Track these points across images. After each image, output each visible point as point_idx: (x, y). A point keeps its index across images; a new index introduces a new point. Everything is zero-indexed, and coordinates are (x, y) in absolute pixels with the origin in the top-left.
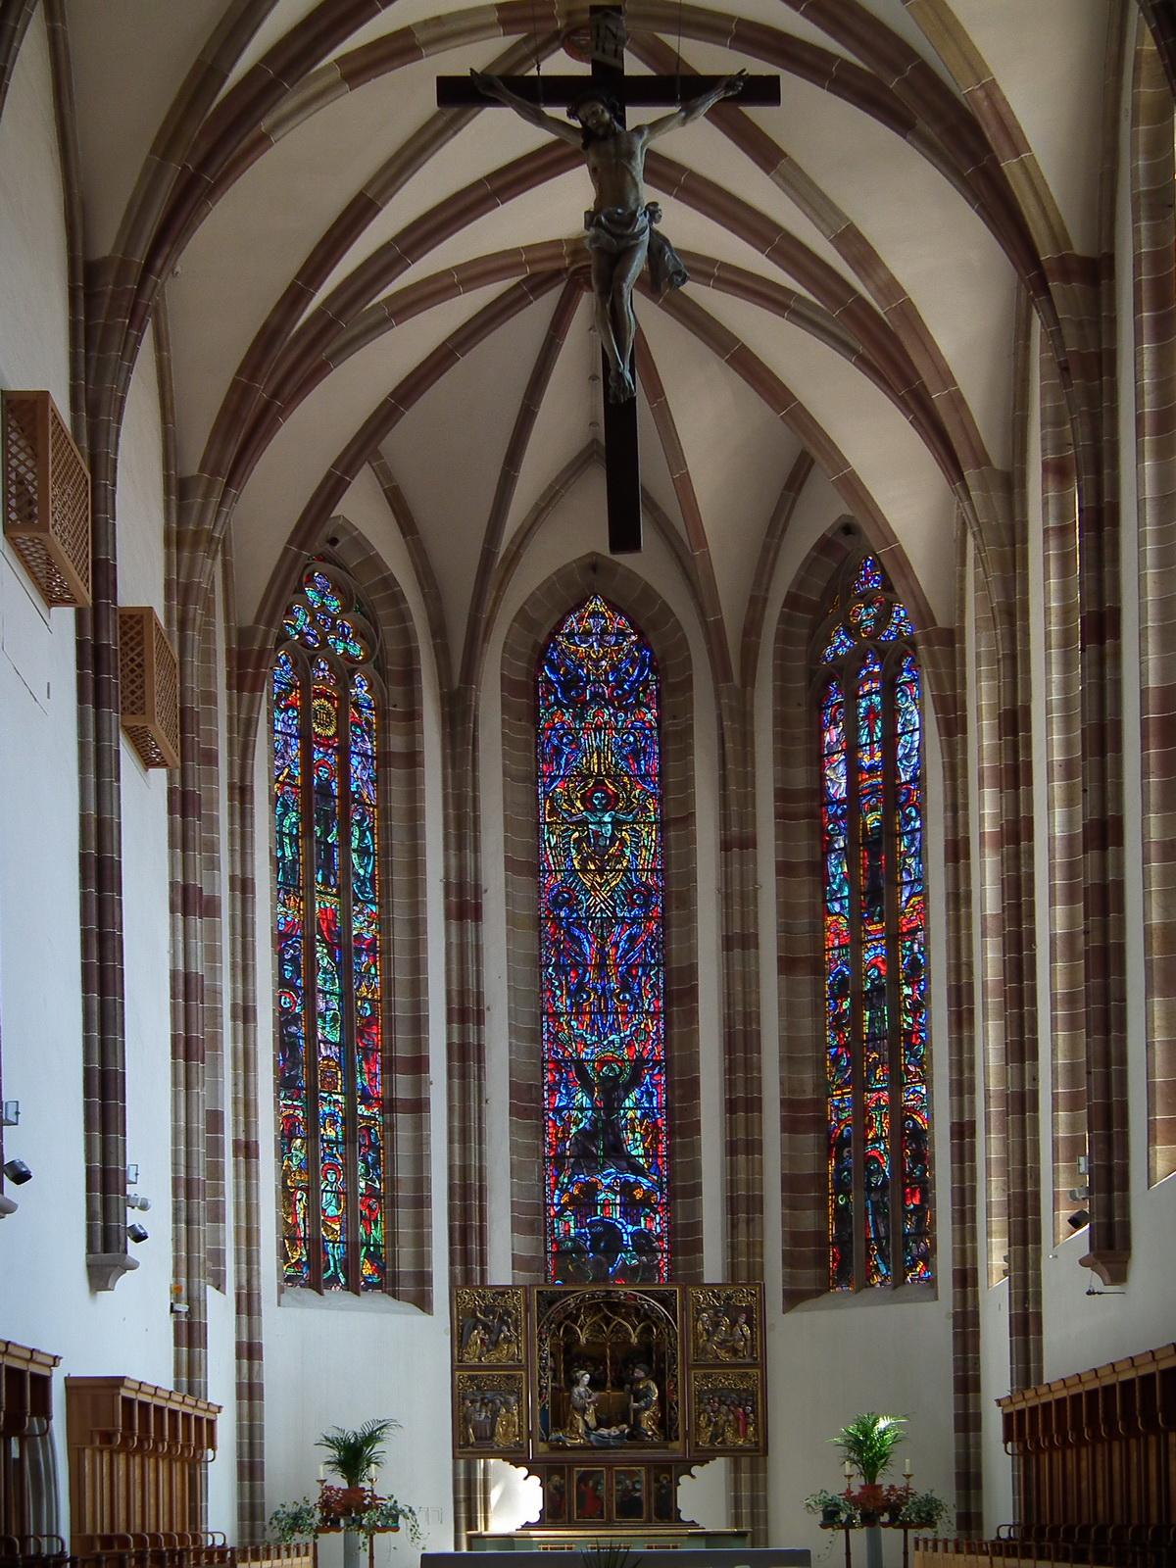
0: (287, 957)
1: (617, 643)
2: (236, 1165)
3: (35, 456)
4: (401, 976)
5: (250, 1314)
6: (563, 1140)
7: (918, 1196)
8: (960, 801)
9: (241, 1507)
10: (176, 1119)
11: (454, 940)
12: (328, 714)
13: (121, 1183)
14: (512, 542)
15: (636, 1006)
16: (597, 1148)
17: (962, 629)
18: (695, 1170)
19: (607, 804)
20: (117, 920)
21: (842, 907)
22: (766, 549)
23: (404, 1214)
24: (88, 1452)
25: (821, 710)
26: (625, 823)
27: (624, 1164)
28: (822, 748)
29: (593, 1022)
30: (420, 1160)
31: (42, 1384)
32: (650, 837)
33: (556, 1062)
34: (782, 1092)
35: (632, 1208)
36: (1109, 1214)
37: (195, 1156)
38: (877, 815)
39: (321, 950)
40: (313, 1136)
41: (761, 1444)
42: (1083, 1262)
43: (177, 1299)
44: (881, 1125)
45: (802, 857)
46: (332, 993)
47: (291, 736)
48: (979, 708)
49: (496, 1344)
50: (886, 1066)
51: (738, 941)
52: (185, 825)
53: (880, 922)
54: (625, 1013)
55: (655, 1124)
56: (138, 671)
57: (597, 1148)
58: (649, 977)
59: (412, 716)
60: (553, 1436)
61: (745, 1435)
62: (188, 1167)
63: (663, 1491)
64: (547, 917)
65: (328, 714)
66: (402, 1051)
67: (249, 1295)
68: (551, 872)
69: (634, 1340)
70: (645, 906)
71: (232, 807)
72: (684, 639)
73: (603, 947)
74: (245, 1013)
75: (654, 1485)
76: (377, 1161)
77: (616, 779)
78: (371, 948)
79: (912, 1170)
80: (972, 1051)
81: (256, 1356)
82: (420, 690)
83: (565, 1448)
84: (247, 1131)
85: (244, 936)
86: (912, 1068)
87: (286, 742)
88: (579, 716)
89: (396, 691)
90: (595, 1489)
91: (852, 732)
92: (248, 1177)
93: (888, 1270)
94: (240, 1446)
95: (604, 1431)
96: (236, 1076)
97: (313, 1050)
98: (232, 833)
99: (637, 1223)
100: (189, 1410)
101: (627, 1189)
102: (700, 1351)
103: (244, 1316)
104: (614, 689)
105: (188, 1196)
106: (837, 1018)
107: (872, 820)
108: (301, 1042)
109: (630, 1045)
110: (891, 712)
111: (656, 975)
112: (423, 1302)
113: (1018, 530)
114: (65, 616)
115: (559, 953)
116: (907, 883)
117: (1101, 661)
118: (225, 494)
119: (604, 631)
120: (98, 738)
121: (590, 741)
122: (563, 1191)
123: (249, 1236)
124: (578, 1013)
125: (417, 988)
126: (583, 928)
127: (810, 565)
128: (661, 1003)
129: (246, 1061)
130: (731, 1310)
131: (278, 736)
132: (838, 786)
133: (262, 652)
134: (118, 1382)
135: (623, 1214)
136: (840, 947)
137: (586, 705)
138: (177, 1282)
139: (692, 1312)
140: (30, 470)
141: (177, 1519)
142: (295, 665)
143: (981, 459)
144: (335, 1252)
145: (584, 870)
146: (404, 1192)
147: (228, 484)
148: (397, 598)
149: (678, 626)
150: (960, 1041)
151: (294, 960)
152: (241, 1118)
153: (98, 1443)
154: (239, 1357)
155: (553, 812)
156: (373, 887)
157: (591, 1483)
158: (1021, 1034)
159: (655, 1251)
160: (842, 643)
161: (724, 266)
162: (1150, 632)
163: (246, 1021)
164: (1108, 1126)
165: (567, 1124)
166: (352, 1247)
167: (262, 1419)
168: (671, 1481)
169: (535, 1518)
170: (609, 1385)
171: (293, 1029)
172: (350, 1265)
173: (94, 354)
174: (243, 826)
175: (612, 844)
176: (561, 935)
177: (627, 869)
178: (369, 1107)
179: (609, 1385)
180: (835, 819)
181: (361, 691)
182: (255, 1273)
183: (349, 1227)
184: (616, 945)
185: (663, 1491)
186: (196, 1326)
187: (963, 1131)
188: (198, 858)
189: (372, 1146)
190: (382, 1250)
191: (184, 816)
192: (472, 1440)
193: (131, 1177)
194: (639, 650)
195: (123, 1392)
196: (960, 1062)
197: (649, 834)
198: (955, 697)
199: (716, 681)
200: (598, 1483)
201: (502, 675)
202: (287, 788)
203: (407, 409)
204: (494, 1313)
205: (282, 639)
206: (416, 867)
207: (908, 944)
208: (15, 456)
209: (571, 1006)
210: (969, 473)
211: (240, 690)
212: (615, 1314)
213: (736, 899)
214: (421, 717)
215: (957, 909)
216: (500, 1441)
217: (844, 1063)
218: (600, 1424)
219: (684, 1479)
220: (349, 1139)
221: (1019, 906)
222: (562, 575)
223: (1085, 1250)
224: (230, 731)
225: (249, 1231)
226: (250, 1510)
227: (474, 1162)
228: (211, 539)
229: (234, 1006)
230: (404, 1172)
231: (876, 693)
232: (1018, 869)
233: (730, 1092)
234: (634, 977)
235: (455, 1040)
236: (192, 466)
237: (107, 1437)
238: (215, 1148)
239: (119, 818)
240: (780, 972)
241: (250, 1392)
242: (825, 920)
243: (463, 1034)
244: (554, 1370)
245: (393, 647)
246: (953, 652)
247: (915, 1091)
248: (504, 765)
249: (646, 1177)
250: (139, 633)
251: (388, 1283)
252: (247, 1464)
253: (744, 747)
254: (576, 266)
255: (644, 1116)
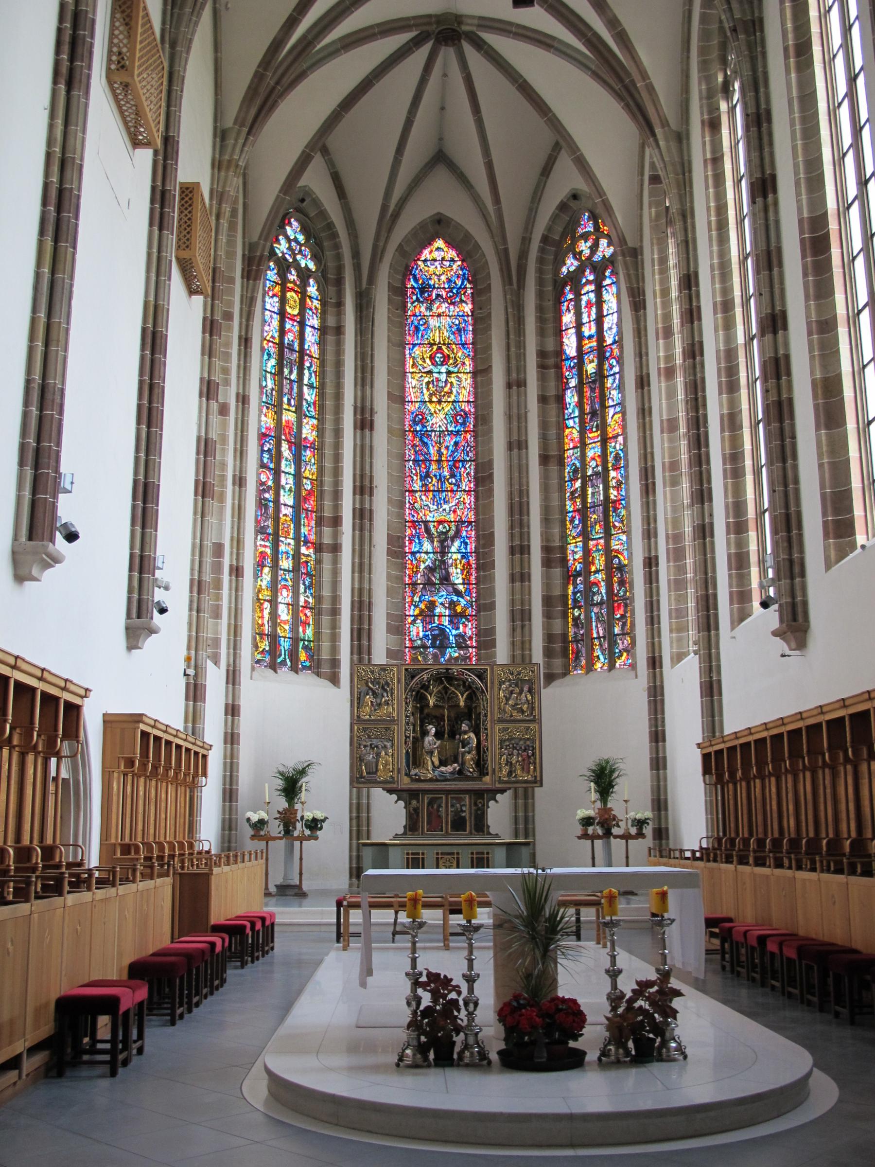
0: (266, 449)
1: (450, 266)
2: (231, 581)
3: (129, 37)
4: (328, 464)
5: (234, 684)
6: (417, 572)
7: (622, 609)
8: (644, 350)
9: (223, 821)
10: (194, 537)
11: (358, 442)
12: (295, 301)
13: (152, 567)
14: (396, 206)
15: (458, 486)
16: (435, 577)
17: (641, 247)
18: (491, 592)
19: (444, 361)
20: (162, 374)
21: (574, 422)
22: (530, 210)
23: (326, 619)
24: (116, 774)
25: (560, 303)
26: (453, 373)
27: (451, 589)
28: (561, 326)
29: (434, 496)
30: (335, 584)
31: (73, 711)
32: (467, 381)
33: (413, 522)
34: (542, 541)
35: (456, 617)
36: (793, 595)
37: (204, 564)
38: (594, 365)
39: (285, 446)
40: (275, 567)
41: (538, 779)
42: (775, 634)
43: (189, 667)
44: (599, 562)
45: (552, 392)
46: (289, 474)
47: (274, 312)
48: (654, 292)
49: (380, 705)
50: (602, 523)
51: (516, 445)
52: (211, 340)
53: (597, 431)
54: (452, 491)
55: (468, 563)
56: (189, 223)
57: (435, 577)
58: (466, 469)
59: (340, 304)
60: (413, 772)
61: (528, 772)
62: (200, 572)
63: (479, 812)
64: (410, 431)
65: (295, 301)
66: (327, 513)
67: (234, 671)
68: (412, 402)
69: (462, 703)
70: (464, 424)
71: (240, 350)
72: (486, 262)
73: (440, 448)
74: (240, 481)
75: (473, 808)
76: (311, 583)
77: (448, 346)
78: (312, 446)
79: (618, 591)
80: (655, 510)
81: (236, 714)
82: (345, 289)
83: (419, 780)
84: (238, 559)
85: (242, 432)
86: (617, 524)
87: (271, 317)
88: (429, 309)
89: (332, 290)
90: (438, 811)
91: (578, 315)
92: (237, 590)
93: (605, 659)
94: (225, 776)
95: (443, 769)
96: (233, 522)
97: (277, 510)
98: (239, 366)
99: (457, 628)
100: (190, 746)
101: (452, 605)
102: (502, 711)
103: (230, 685)
104: (448, 292)
105: (199, 593)
106: (572, 493)
107: (591, 368)
108: (271, 504)
109: (455, 512)
110: (600, 302)
111: (471, 468)
112: (334, 680)
113: (686, 165)
114: (145, 156)
115: (416, 452)
116: (612, 406)
117: (766, 209)
118: (246, 139)
119: (443, 259)
120: (159, 251)
121: (433, 322)
122: (416, 607)
123: (235, 630)
124: (426, 491)
125: (337, 472)
126: (429, 436)
127: (554, 218)
128: (472, 485)
129: (239, 512)
130: (519, 683)
131: (267, 313)
132: (570, 345)
133: (261, 256)
134: (138, 718)
135: (451, 622)
136: (574, 448)
137: (432, 302)
138: (189, 653)
139: (496, 683)
140: (125, 46)
141: (821, 777)
142: (279, 271)
143: (665, 124)
144: (285, 644)
145: (431, 402)
146: (326, 605)
147: (249, 133)
148: (334, 236)
149: (483, 255)
150: (648, 503)
151: (269, 450)
152: (235, 550)
153: (122, 767)
154: (226, 714)
155: (414, 365)
156: (315, 408)
157: (435, 807)
158: (701, 484)
159: (467, 647)
160: (572, 264)
161: (518, 26)
162: (802, 181)
163: (240, 486)
164: (789, 530)
165: (419, 561)
166: (295, 640)
167: (238, 759)
168: (483, 805)
169: (401, 831)
170: (446, 736)
171: (267, 495)
172: (293, 654)
173: (176, 10)
174: (245, 362)
175: (446, 385)
176: (417, 441)
177: (454, 401)
178: (308, 548)
179: (446, 736)
180: (570, 369)
181: (312, 290)
182: (238, 656)
183: (294, 629)
184: (447, 448)
185: (479, 812)
186: (199, 686)
187: (651, 562)
188: (218, 363)
189: (308, 574)
190: (312, 644)
191: (211, 335)
192: (365, 774)
193: (159, 563)
194: (462, 270)
195: (142, 727)
196: (648, 517)
197: (466, 380)
198: (638, 288)
199: (504, 286)
200: (440, 806)
201: (389, 283)
202: (271, 344)
203: (346, 113)
204: (379, 683)
205: (273, 253)
206: (338, 396)
207: (613, 444)
208: (117, 37)
209: (422, 486)
210: (658, 131)
211: (248, 280)
212: (451, 685)
213: (515, 418)
214: (344, 305)
215: (644, 418)
216: (382, 776)
217: (577, 522)
218: (443, 763)
219: (491, 803)
220: (296, 569)
221: (696, 399)
222: (422, 226)
223: (775, 624)
224: (242, 303)
225: (236, 626)
226: (228, 825)
227: (366, 586)
228: (237, 166)
229: (234, 476)
230: (326, 592)
231: (592, 291)
232: (695, 375)
233: (512, 541)
234: (457, 468)
235: (358, 506)
236: (229, 122)
237: (130, 762)
238: (217, 568)
239: (168, 305)
240: (540, 465)
241: (231, 738)
242: (564, 432)
243: (362, 502)
244: (414, 725)
245: (331, 264)
246: (636, 263)
247: (620, 539)
248: (389, 336)
249: (463, 598)
250: (190, 199)
251: (316, 667)
252: (228, 791)
253: (519, 325)
254: (440, 29)
255: (463, 557)
